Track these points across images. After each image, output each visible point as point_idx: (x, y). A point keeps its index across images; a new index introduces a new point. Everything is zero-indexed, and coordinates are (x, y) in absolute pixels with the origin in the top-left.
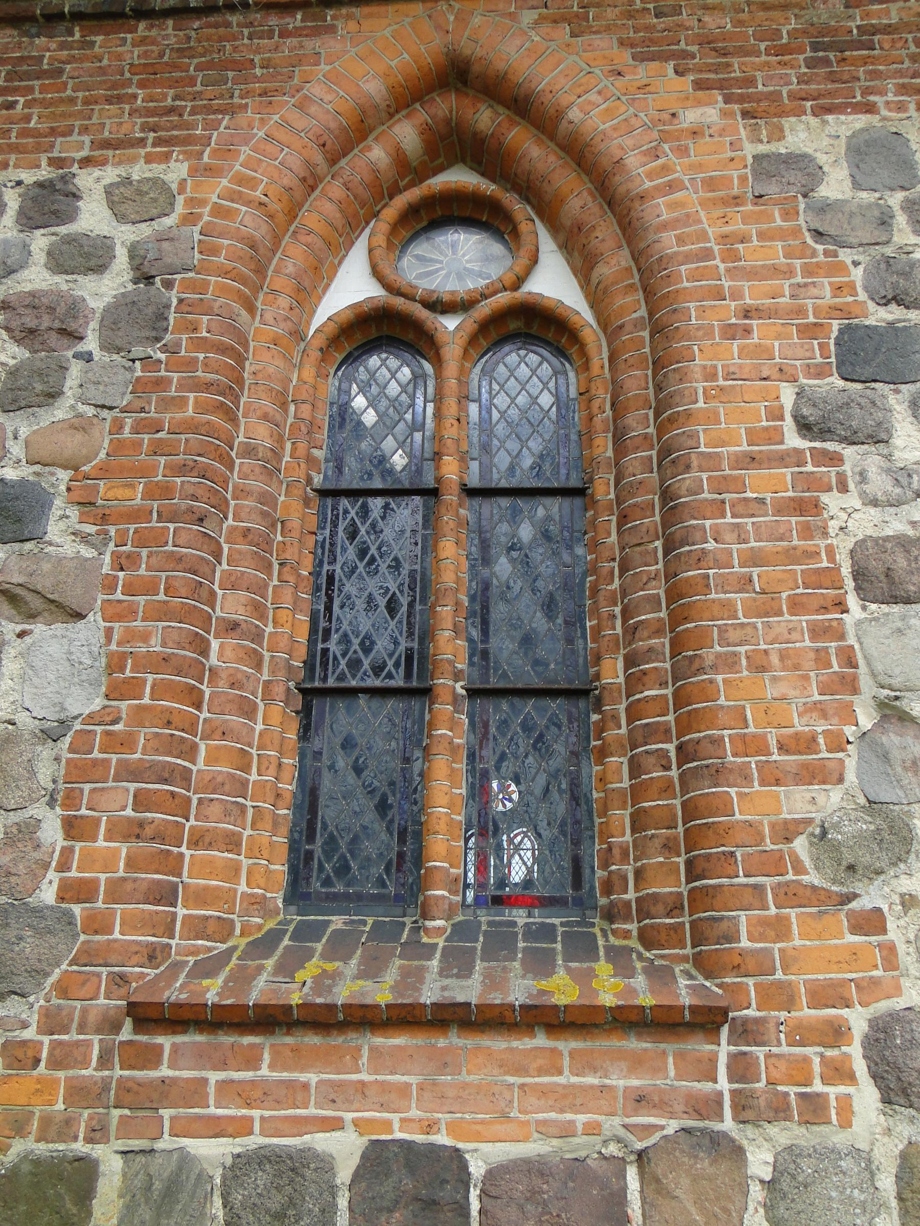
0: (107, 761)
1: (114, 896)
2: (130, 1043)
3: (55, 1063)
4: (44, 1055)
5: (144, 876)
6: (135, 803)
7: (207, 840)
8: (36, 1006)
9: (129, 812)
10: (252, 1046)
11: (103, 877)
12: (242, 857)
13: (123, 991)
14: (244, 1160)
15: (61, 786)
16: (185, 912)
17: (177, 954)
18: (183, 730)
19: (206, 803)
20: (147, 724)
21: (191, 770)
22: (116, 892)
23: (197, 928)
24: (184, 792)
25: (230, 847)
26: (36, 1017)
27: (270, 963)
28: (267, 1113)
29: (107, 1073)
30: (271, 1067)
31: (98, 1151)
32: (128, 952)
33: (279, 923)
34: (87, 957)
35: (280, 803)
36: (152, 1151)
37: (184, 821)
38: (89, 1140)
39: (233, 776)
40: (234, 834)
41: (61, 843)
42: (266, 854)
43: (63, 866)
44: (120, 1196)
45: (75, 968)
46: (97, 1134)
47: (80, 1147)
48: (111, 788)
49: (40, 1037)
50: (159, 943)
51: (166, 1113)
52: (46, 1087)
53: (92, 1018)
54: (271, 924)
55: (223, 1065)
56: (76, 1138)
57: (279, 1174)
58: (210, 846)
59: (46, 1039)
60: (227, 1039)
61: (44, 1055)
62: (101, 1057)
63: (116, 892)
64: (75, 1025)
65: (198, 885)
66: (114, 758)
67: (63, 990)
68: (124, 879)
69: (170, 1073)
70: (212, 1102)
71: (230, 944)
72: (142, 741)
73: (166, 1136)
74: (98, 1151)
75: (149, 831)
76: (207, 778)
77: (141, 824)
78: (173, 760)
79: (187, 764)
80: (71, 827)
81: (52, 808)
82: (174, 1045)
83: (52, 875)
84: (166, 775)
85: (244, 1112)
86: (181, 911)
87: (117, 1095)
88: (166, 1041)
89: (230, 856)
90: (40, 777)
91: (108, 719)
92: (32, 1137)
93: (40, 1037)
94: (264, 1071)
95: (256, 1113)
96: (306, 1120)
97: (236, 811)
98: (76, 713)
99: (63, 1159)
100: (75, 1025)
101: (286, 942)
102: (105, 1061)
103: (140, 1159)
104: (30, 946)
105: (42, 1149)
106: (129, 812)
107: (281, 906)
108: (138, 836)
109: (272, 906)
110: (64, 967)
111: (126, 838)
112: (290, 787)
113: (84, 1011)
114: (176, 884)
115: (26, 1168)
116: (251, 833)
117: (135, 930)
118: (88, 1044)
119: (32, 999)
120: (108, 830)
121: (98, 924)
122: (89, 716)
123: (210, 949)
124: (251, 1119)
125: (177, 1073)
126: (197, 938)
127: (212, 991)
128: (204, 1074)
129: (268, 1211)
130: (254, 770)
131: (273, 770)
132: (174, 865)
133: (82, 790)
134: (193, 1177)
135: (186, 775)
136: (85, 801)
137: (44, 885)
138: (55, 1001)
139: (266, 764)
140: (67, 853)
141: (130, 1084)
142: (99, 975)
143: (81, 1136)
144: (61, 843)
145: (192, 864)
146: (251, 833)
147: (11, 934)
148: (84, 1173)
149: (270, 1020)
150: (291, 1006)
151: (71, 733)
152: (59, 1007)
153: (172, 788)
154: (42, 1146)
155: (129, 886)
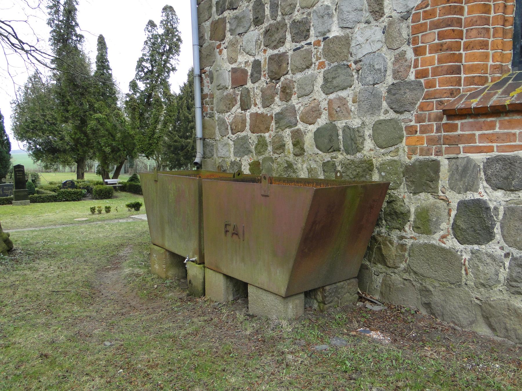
0: (426, 23)
1: (435, 74)
2: (446, 124)
3: (422, 132)
4: (418, 129)
5: (445, 64)
6: (438, 37)
7: (471, 46)
8: (414, 114)
9: (437, 41)
10: (491, 121)
11: (430, 67)
12: (489, 50)
13: (442, 107)
14: (491, 160)
15: (411, 37)
16: (465, 76)
17: (463, 92)
18: (455, 2)
19: (470, 31)
20: (439, 4)
21: (461, 19)
22: (435, 72)
23: (470, 81)
24: (459, 28)
25: (482, 47)
26: (414, 118)
27: (500, 91)
28: (499, 144)
29: (439, 134)
30: (500, 128)
31: (439, 158)
32: (442, 93)
33: (509, 75)
34: (428, 96)
35: (507, 24)
36: (458, 158)
37: (460, 40)
38: (436, 155)
39: (481, 17)
40: (483, 41)
41: (414, 58)
42: (500, 47)
43: (416, 66)
44: (449, 172)
45: (424, 101)
46: (439, 153)
47: (433, 157)
48: (429, 33)
49: (416, 124)
50: (454, 88)
51: (461, 146)
52: (420, 139)
53: (432, 116)
54: (506, 76)
55: (481, 129)
56: (432, 155)
57: (505, 165)
58: (473, 48)
59: (418, 125)
60: (482, 120)
61: (418, 129)
62: (437, 129)
63: (435, 72)
64: (427, 119)
65: (469, 65)
66: (428, 21)
67: (421, 108)
68: (437, 67)
69: (461, 133)
70: (477, 141)
71: (486, 86)
72: (438, 11)
73: (462, 153)
74: (439, 158)
75: (445, 47)
76: (469, 20)
77: (442, 45)
78: (452, 16)
79: (459, 16)
80: (418, 51)
81: (409, 46)
82: (462, 123)
83: (412, 70)
84: (449, 23)
85: (490, 144)
86: (463, 76)
87: (443, 141)
88: (459, 122)
89: (483, 51)
90: (403, 35)
91: (424, 6)
92: (418, 154)
93: (416, 124)
94: (497, 130)
95: (495, 145)
96: (515, 146)
97: (484, 31)
98: (412, 7)
99: (428, 160)
100: (427, 119)
101: (510, 82)
102: (438, 130)
103: (454, 160)
104: (409, 95)
105: (421, 158)
106: (437, 41)
107: (510, 68)
108: (441, 50)
109: (506, 69)
110: (421, 101)
111: (436, 52)
112: (512, 16)
113: (429, 114)
114: (460, 66)
115: (417, 163)
116: (493, 39)
117: (444, 85)
118: (432, 125)
119: (412, 112)
120: (430, 50)
121: (430, 85)
122: (417, 7)
123: (476, 89)
124: (493, 147)
125: (464, 133)
126: (470, 85)
127: (474, 103)
128: (474, 132)
129: (501, 177)
130: (492, 11)
131: (501, 10)
132: (459, 58)
133: (418, 37)
134: (472, 166)
135: (459, 22)
136: (420, 41)
137: (410, 74)
138: (419, 112)
139: (497, 8)
140: (416, 61)
141: (447, 137)
142: (433, 102)
143: (433, 154)
144: (414, 58)
145: (466, 57)
146: (493, 39)
147: (402, 92)
148: (435, 166)
149: (498, 111)
150: (505, 105)
151: (411, 15)
152: (421, 114)
153: (452, 28)
154: (421, 157)
155: (440, 69)
